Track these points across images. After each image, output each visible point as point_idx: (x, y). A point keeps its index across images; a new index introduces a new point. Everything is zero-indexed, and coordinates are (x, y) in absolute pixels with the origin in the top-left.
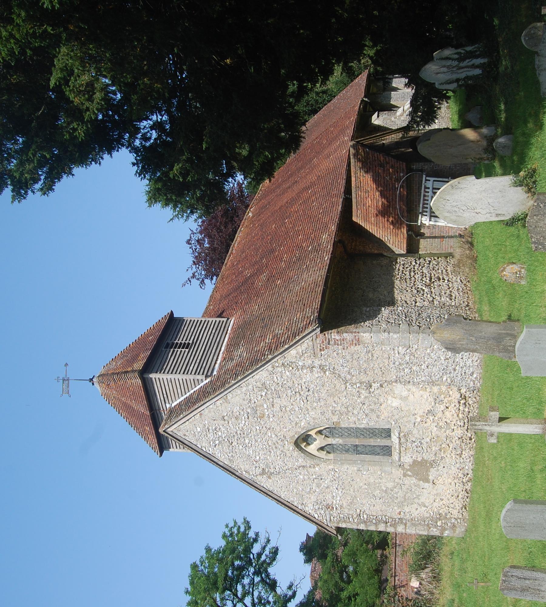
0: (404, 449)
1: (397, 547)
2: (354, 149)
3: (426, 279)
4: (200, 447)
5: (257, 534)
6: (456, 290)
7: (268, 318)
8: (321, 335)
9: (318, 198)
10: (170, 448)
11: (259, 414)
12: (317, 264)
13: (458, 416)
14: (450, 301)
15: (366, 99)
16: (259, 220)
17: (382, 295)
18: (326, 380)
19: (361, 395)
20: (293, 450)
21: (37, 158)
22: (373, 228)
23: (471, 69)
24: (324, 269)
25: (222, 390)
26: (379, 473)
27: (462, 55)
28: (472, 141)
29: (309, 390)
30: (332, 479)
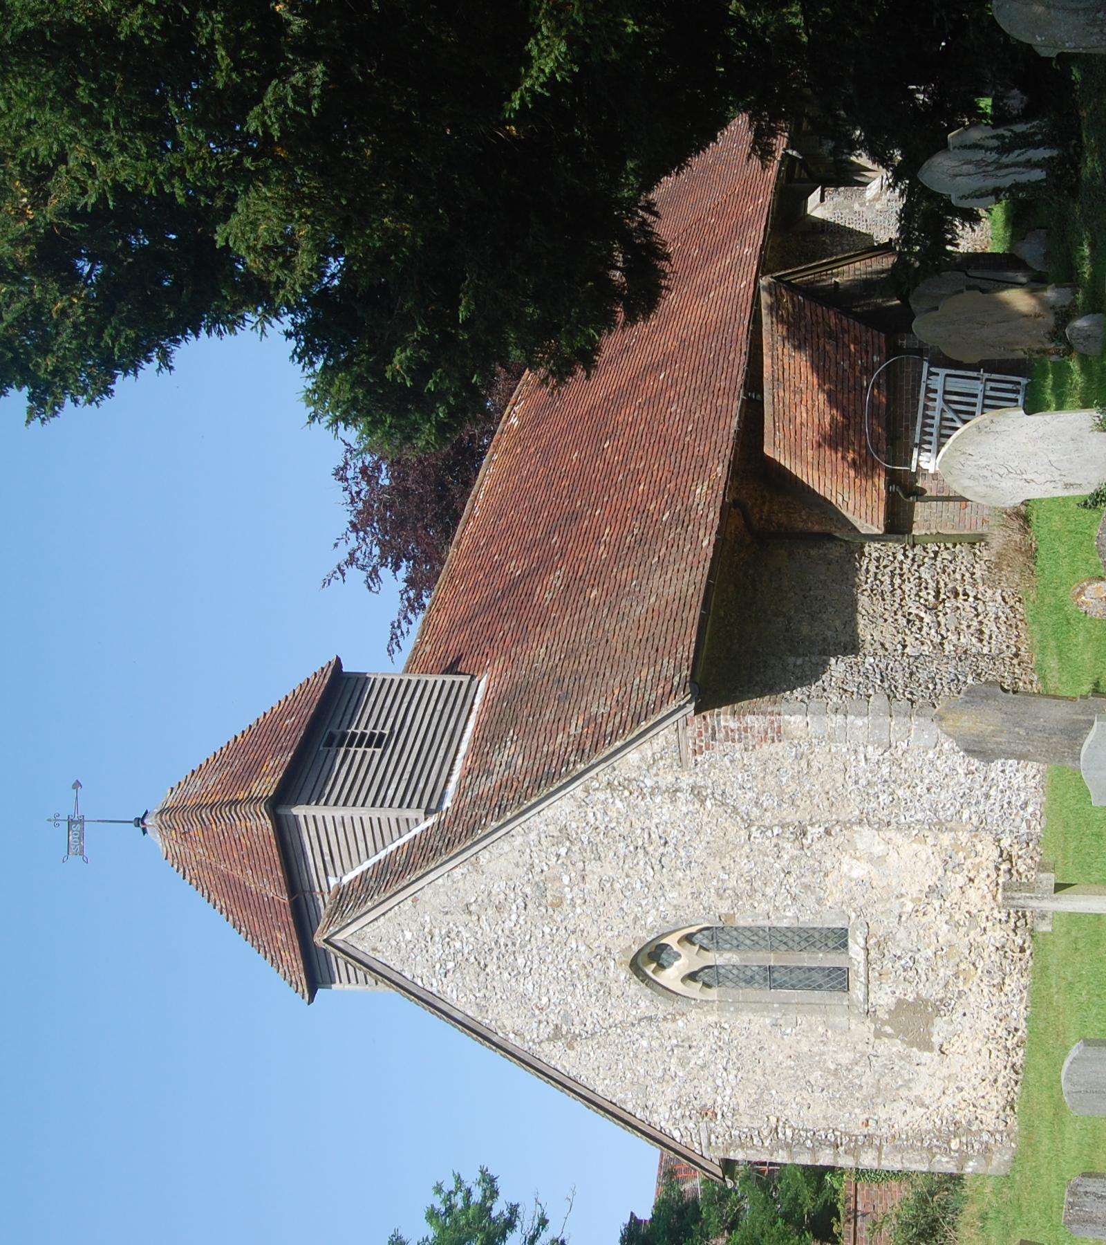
0: (877, 974)
1: (859, 1219)
2: (771, 294)
3: (928, 594)
4: (410, 977)
5: (513, 1210)
6: (992, 619)
7: (573, 678)
8: (697, 720)
9: (682, 394)
10: (333, 982)
11: (550, 898)
12: (685, 555)
13: (994, 898)
14: (979, 644)
15: (794, 153)
16: (538, 438)
17: (829, 629)
18: (706, 819)
19: (782, 853)
20: (627, 980)
21: (120, 344)
22: (810, 473)
23: (1024, 170)
24: (701, 569)
25: (468, 843)
26: (821, 1030)
27: (1007, 140)
28: (1026, 316)
29: (666, 843)
30: (714, 1047)
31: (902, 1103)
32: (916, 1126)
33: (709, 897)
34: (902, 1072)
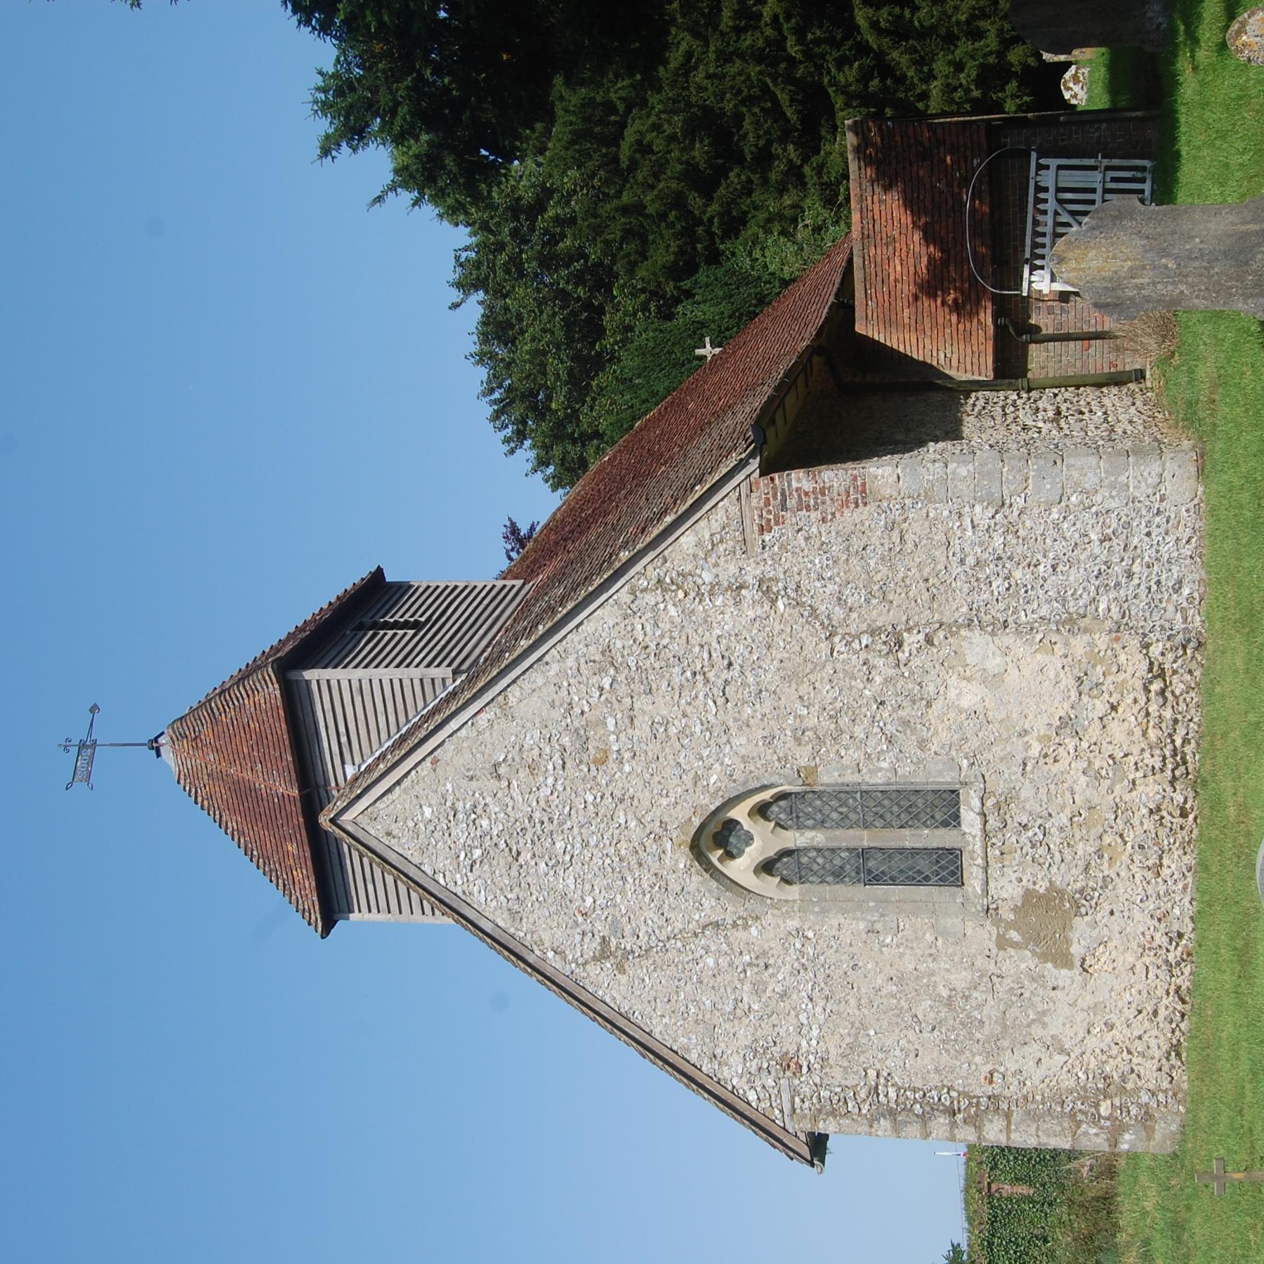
0: (997, 852)
2: (857, 134)
4: (430, 873)
8: (764, 481)
11: (592, 751)
13: (1144, 733)
19: (873, 673)
20: (688, 869)
29: (730, 664)
30: (796, 965)
31: (1036, 1047)
32: (1054, 1083)
33: (785, 743)
34: (1034, 999)
